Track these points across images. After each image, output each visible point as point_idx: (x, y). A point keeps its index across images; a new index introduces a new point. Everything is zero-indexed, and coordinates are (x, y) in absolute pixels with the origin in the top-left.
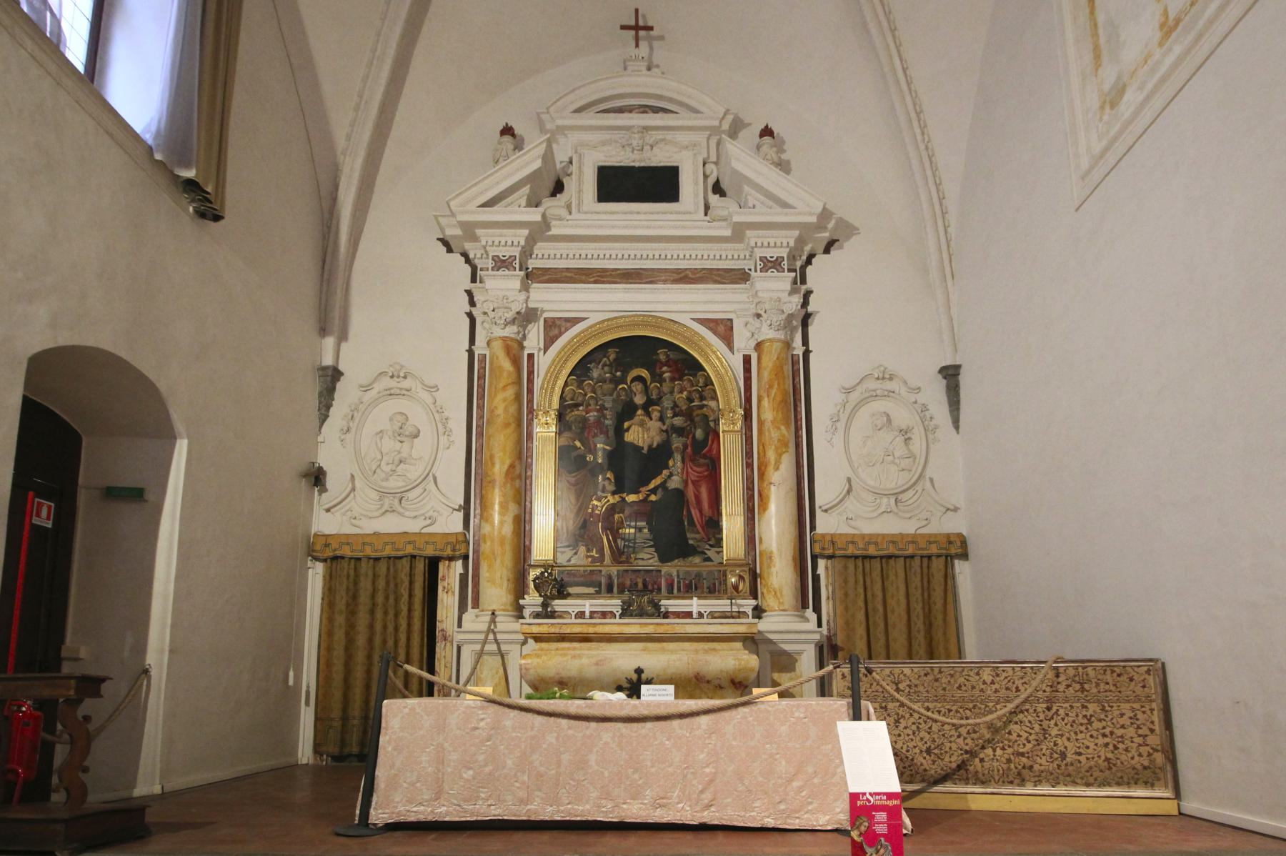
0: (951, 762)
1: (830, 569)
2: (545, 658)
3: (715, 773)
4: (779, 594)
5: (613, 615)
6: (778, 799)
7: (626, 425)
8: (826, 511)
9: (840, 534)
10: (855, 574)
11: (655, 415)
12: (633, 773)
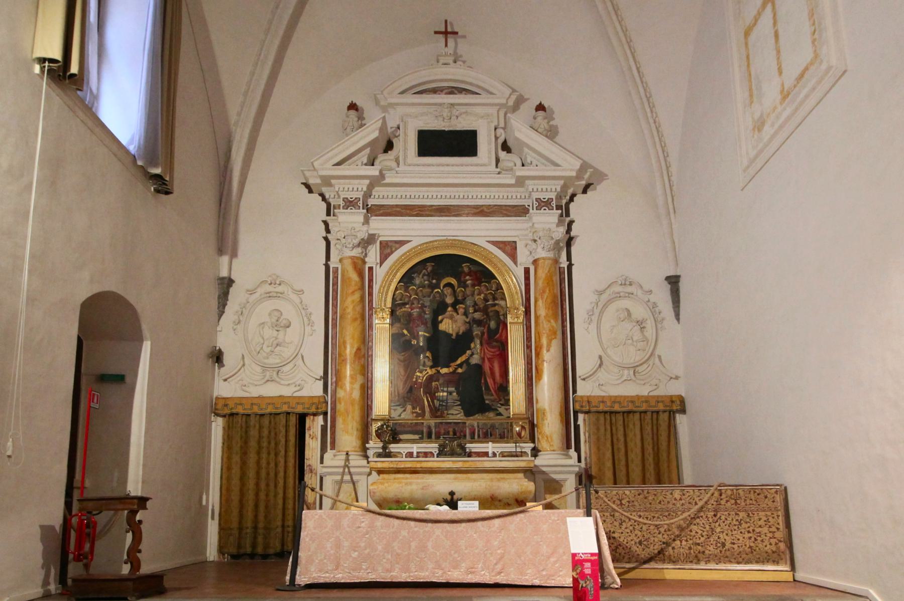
0: (654, 550)
1: (587, 420)
2: (386, 485)
3: (504, 553)
4: (550, 440)
5: (432, 454)
6: (541, 568)
7: (440, 318)
8: (584, 379)
9: (594, 396)
10: (605, 425)
11: (461, 311)
12: (455, 553)
